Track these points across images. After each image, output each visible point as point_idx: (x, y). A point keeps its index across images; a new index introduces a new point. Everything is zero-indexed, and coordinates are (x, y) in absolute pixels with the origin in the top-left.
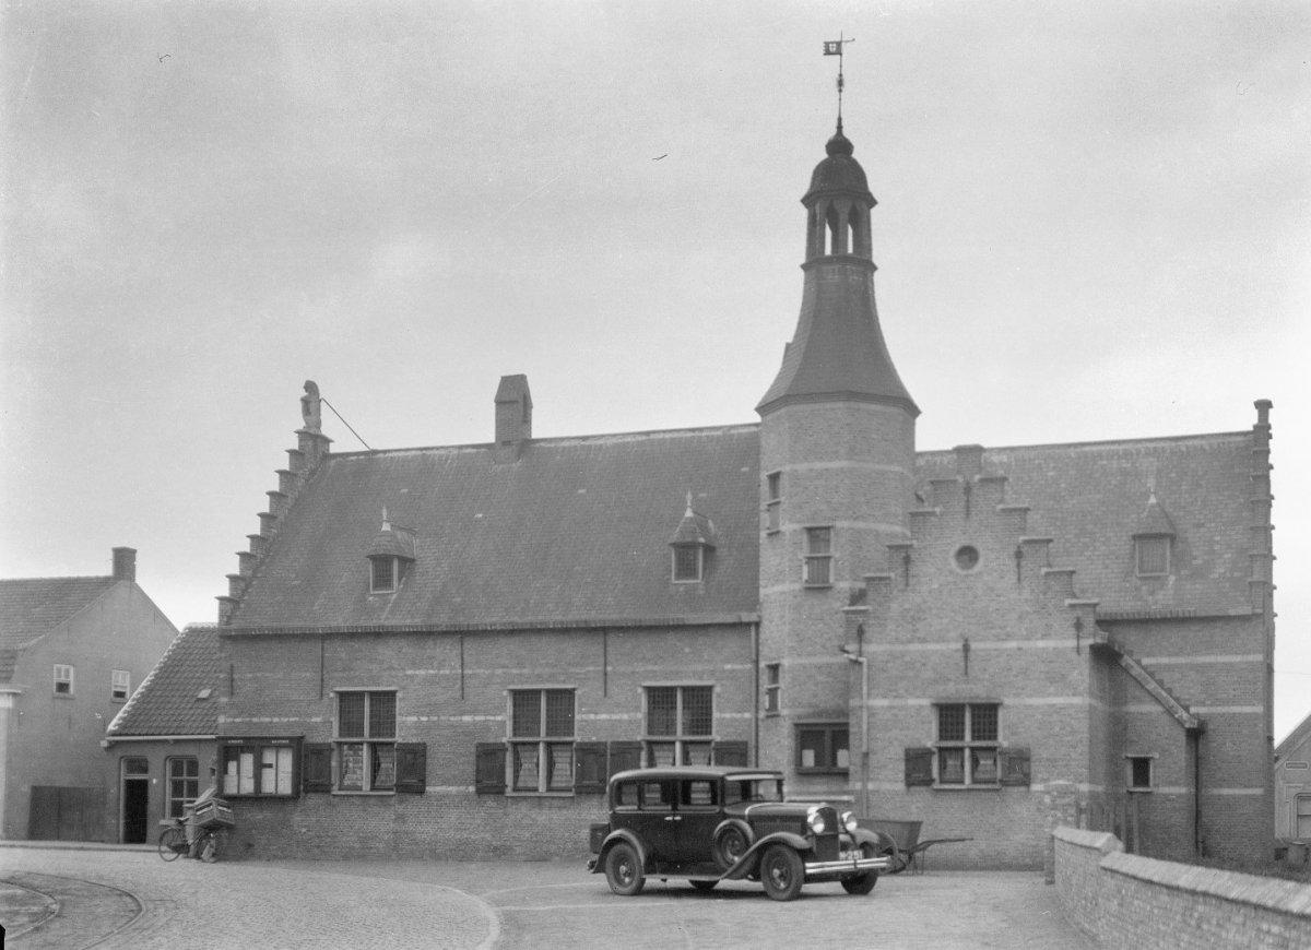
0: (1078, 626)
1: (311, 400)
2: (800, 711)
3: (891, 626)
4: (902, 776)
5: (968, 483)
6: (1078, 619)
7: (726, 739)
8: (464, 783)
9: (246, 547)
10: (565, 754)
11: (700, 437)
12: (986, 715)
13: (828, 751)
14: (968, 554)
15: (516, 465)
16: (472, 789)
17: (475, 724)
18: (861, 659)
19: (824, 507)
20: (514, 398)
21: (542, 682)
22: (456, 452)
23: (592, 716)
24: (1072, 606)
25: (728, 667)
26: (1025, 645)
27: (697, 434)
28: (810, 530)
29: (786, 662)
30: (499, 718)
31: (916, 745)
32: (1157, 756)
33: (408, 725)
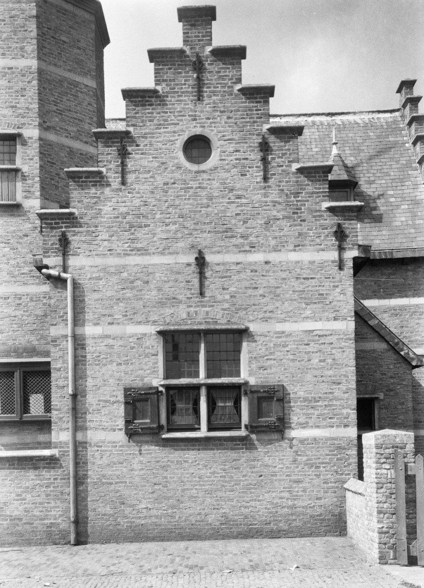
4: (121, 423)
5: (198, 57)
6: (339, 225)
18: (64, 275)
26: (273, 257)
31: (138, 384)
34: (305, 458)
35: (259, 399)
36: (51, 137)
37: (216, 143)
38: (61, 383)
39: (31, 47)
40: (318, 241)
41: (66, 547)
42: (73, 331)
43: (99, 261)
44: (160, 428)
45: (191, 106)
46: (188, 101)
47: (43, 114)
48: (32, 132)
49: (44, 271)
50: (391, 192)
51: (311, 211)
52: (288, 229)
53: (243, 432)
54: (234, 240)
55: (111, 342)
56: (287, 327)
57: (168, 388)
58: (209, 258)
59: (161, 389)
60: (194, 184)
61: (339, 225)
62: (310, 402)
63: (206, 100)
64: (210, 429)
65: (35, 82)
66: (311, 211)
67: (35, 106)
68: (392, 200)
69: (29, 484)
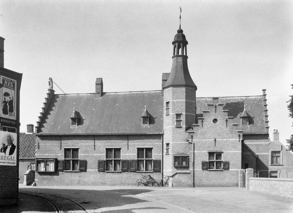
0: (239, 136)
1: (51, 82)
2: (174, 153)
3: (199, 135)
4: (201, 167)
5: (216, 105)
6: (239, 134)
7: (155, 159)
8: (95, 169)
9: (40, 115)
10: (118, 162)
11: (143, 93)
12: (219, 155)
13: (181, 162)
14: (215, 121)
15: (101, 98)
16: (97, 170)
17: (97, 156)
18: (192, 142)
19: (180, 109)
20: (100, 83)
21: (113, 147)
22: (86, 95)
23: (125, 154)
24: (238, 132)
25: (156, 144)
26: (228, 140)
27: (142, 92)
28: (176, 114)
29: (171, 143)
30: (103, 154)
31: (204, 161)
32: (250, 163)
33: (81, 156)
34: (232, 174)
35: (225, 164)
36: (188, 113)
37: (218, 120)
38: (191, 160)
39: (184, 97)
40: (236, 137)
41: (192, 188)
42: (193, 152)
43: (198, 140)
44: (208, 168)
45: (214, 113)
46: (214, 113)
47: (186, 109)
48: (184, 113)
49: (189, 142)
50: (257, 118)
51: (234, 132)
52: (230, 135)
53: (222, 169)
54: (221, 137)
55: (200, 154)
56: (230, 152)
57: (209, 161)
58: (216, 139)
59: (208, 162)
60: (215, 127)
61: (239, 134)
62: (234, 164)
63: (217, 113)
64: (216, 169)
65: (185, 104)
66: (234, 132)
67: (185, 108)
68: (258, 120)
69: (186, 177)
